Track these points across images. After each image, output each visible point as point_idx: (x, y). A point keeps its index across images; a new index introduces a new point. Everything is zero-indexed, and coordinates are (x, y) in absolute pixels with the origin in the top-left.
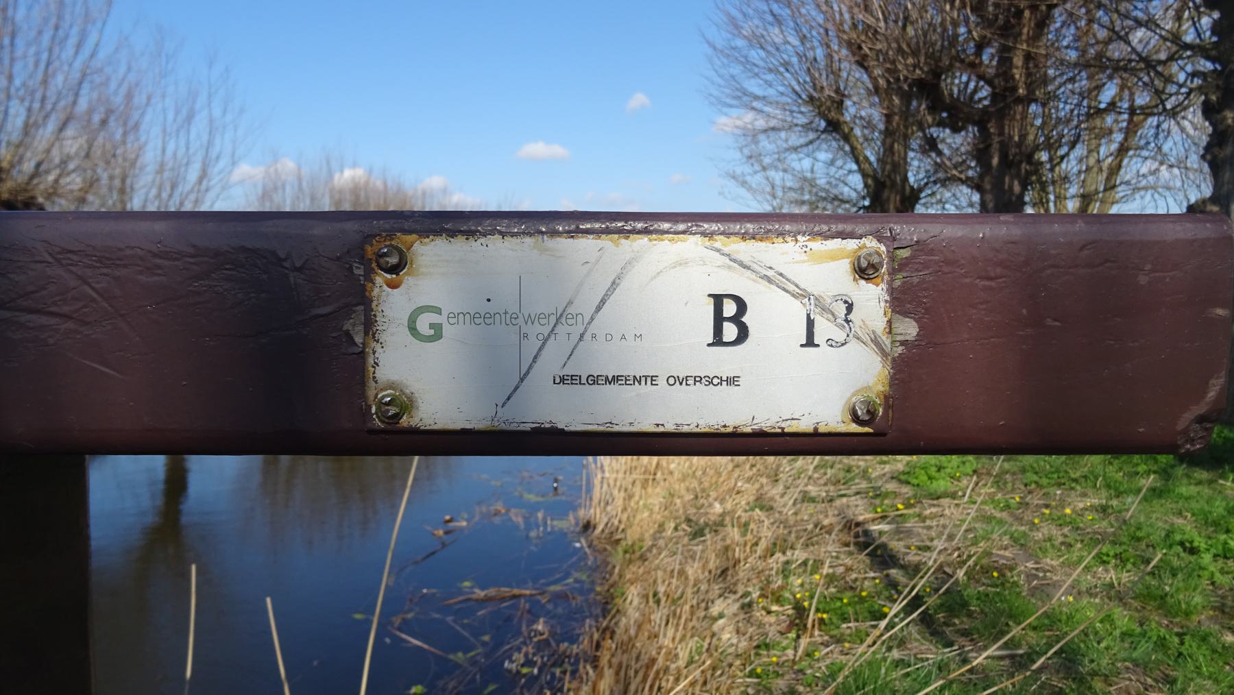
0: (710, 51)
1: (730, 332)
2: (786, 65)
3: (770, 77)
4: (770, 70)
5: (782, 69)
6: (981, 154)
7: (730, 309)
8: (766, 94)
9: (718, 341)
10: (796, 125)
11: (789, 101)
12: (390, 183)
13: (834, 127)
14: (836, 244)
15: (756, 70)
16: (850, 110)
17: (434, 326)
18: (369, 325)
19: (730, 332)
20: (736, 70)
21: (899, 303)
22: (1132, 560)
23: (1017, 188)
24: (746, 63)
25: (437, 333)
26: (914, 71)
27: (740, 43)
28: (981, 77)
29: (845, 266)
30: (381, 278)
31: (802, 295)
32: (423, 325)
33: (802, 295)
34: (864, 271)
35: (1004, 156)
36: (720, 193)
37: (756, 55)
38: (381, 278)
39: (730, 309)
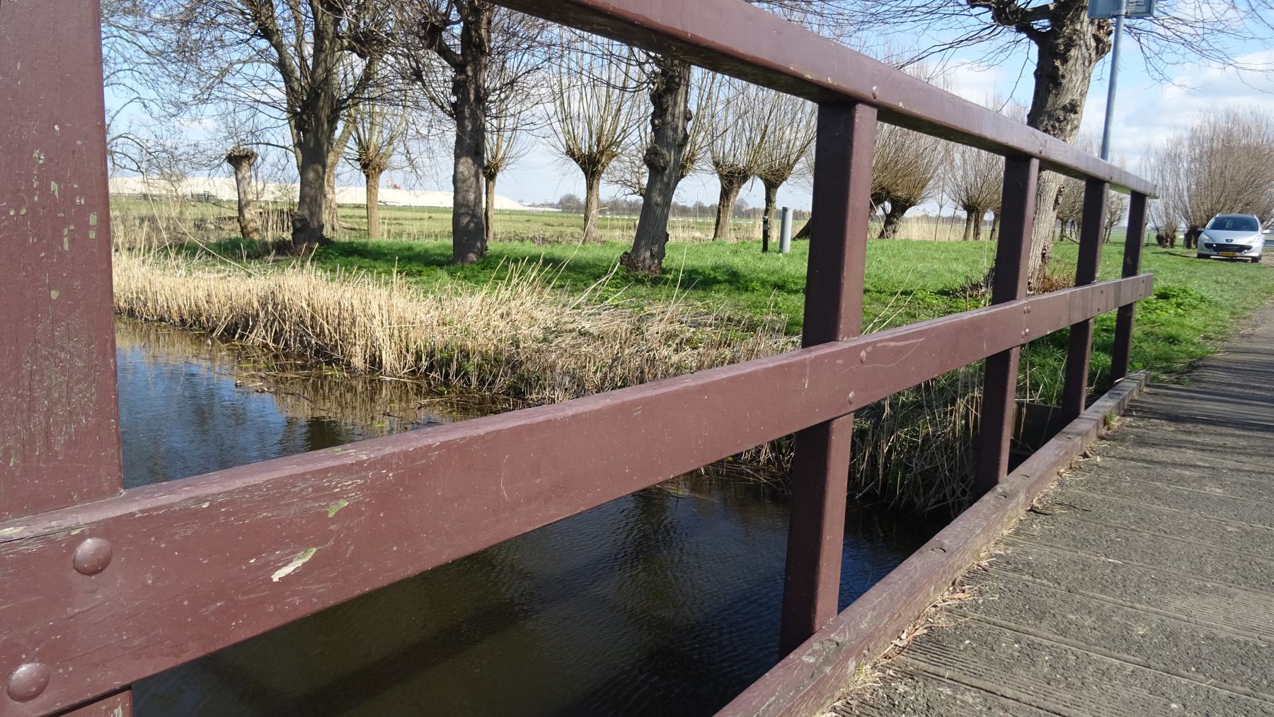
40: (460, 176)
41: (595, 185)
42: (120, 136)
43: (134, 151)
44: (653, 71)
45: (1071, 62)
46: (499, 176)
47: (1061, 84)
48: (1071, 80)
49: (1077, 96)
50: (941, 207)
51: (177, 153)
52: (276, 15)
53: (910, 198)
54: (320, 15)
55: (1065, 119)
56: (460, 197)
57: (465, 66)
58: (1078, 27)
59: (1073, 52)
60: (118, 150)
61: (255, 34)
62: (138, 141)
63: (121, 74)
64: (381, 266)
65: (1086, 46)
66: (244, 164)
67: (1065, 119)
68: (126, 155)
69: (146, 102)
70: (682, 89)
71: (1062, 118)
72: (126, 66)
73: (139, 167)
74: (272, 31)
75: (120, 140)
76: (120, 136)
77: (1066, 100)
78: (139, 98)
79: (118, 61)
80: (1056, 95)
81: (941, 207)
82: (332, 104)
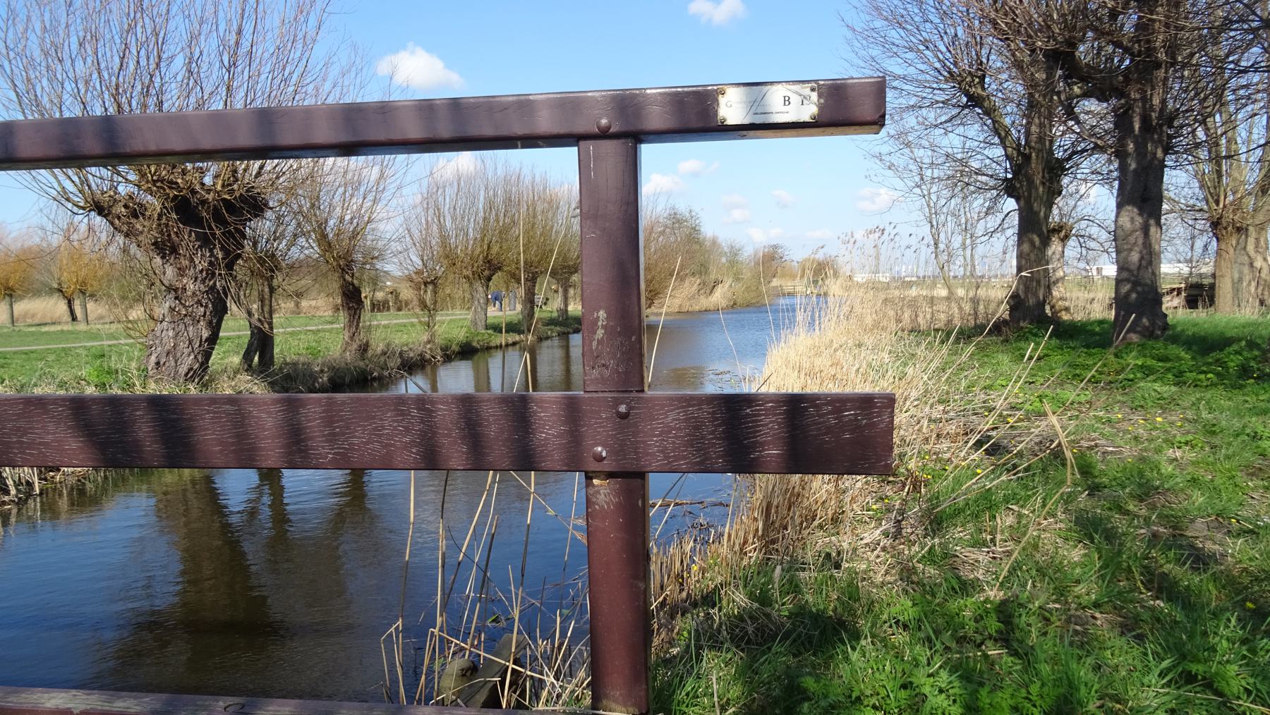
0: (849, 34)
1: (787, 103)
2: (926, 43)
3: (910, 55)
4: (911, 49)
5: (922, 47)
6: (1122, 120)
7: (787, 98)
8: (906, 73)
9: (785, 104)
10: (937, 102)
11: (928, 77)
12: (538, 179)
13: (975, 101)
14: (806, 85)
15: (895, 49)
16: (991, 84)
17: (731, 106)
18: (718, 104)
19: (787, 103)
20: (876, 52)
21: (820, 96)
22: (1200, 445)
23: (1160, 153)
24: (886, 44)
25: (731, 106)
26: (1048, 41)
27: (879, 24)
28: (1117, 44)
29: (809, 89)
30: (720, 96)
31: (801, 95)
32: (729, 104)
33: (801, 95)
34: (813, 90)
35: (1145, 120)
36: (866, 177)
37: (894, 35)
38: (720, 96)
39: (787, 98)
66: (1053, 239)
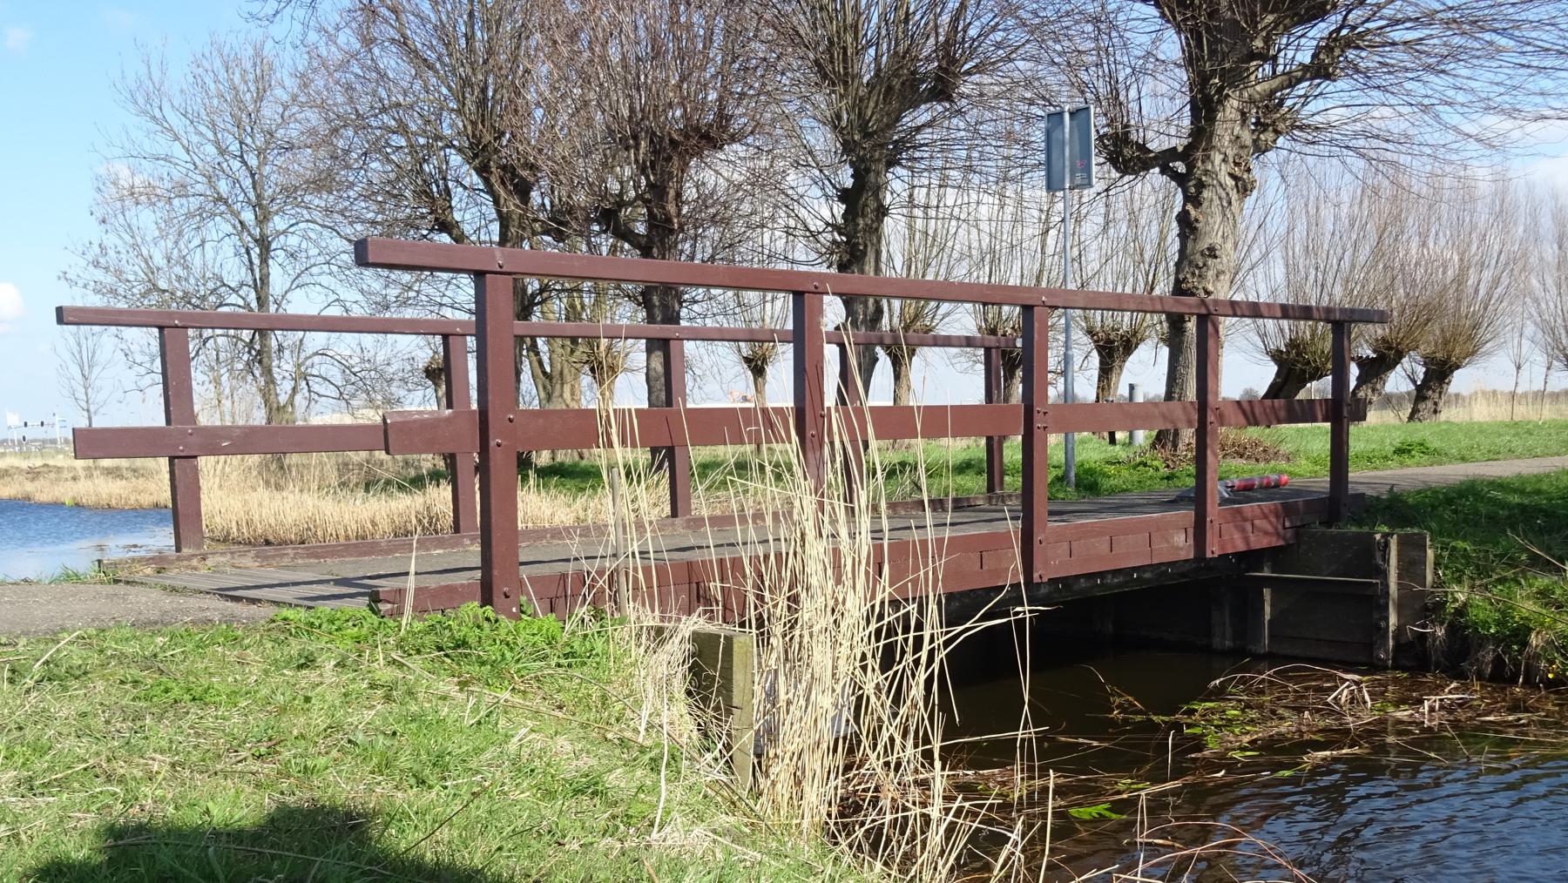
40: (652, 373)
41: (903, 374)
42: (317, 354)
43: (335, 374)
44: (834, 242)
45: (1205, 204)
46: (769, 370)
47: (1196, 228)
48: (1207, 223)
49: (1219, 240)
50: (1519, 368)
51: (391, 370)
52: (453, 204)
53: (1449, 357)
54: (502, 201)
55: (1205, 265)
56: (654, 397)
57: (651, 248)
58: (1210, 167)
59: (1206, 194)
60: (315, 372)
61: (432, 230)
62: (338, 358)
63: (315, 270)
64: (570, 483)
65: (1221, 185)
67: (1205, 265)
68: (325, 379)
69: (348, 304)
70: (871, 257)
71: (1201, 264)
72: (321, 259)
73: (341, 394)
74: (451, 223)
75: (317, 359)
76: (317, 354)
77: (1204, 245)
78: (338, 300)
79: (311, 253)
80: (1195, 240)
81: (1519, 368)
82: (523, 299)
